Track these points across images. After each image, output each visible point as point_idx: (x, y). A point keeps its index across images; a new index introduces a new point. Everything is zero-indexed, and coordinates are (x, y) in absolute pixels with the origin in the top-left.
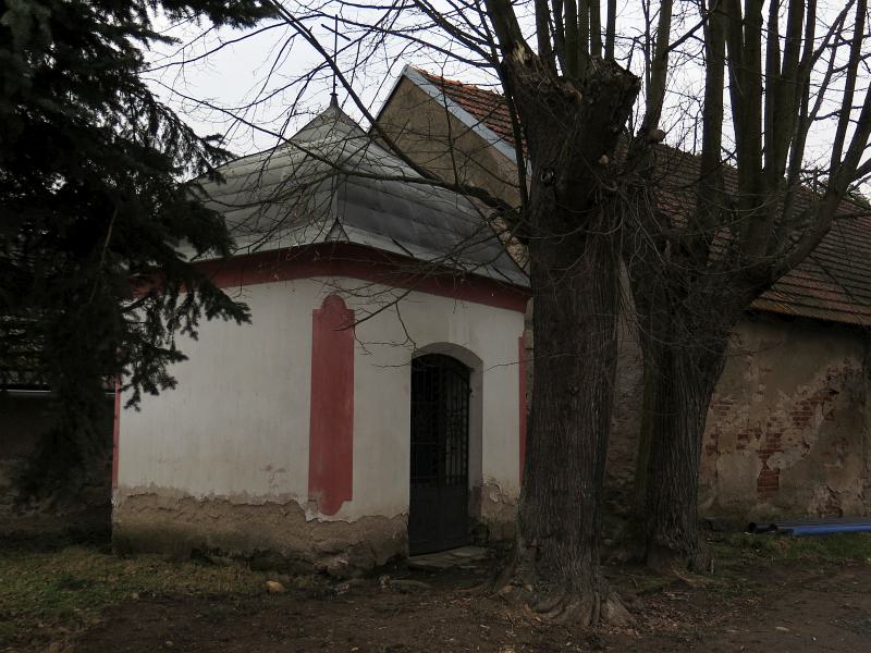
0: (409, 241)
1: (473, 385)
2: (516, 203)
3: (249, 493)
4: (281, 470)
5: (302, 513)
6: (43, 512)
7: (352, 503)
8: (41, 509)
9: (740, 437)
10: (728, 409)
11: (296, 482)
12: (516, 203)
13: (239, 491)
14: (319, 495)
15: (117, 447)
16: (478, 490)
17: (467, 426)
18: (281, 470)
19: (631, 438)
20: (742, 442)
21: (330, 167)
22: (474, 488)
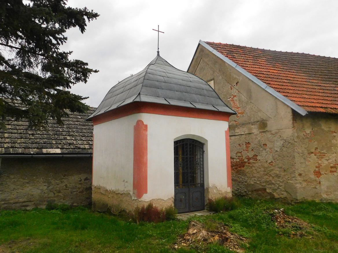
0: (149, 67)
1: (205, 149)
2: (70, 84)
3: (119, 189)
4: (127, 182)
5: (131, 197)
6: (79, 192)
7: (147, 195)
8: (78, 191)
9: (332, 167)
10: (324, 155)
11: (129, 188)
12: (70, 84)
13: (117, 189)
14: (136, 191)
15: (146, 163)
16: (208, 189)
17: (203, 165)
18: (127, 182)
19: (280, 168)
20: (333, 169)
21: (18, 50)
22: (206, 188)
